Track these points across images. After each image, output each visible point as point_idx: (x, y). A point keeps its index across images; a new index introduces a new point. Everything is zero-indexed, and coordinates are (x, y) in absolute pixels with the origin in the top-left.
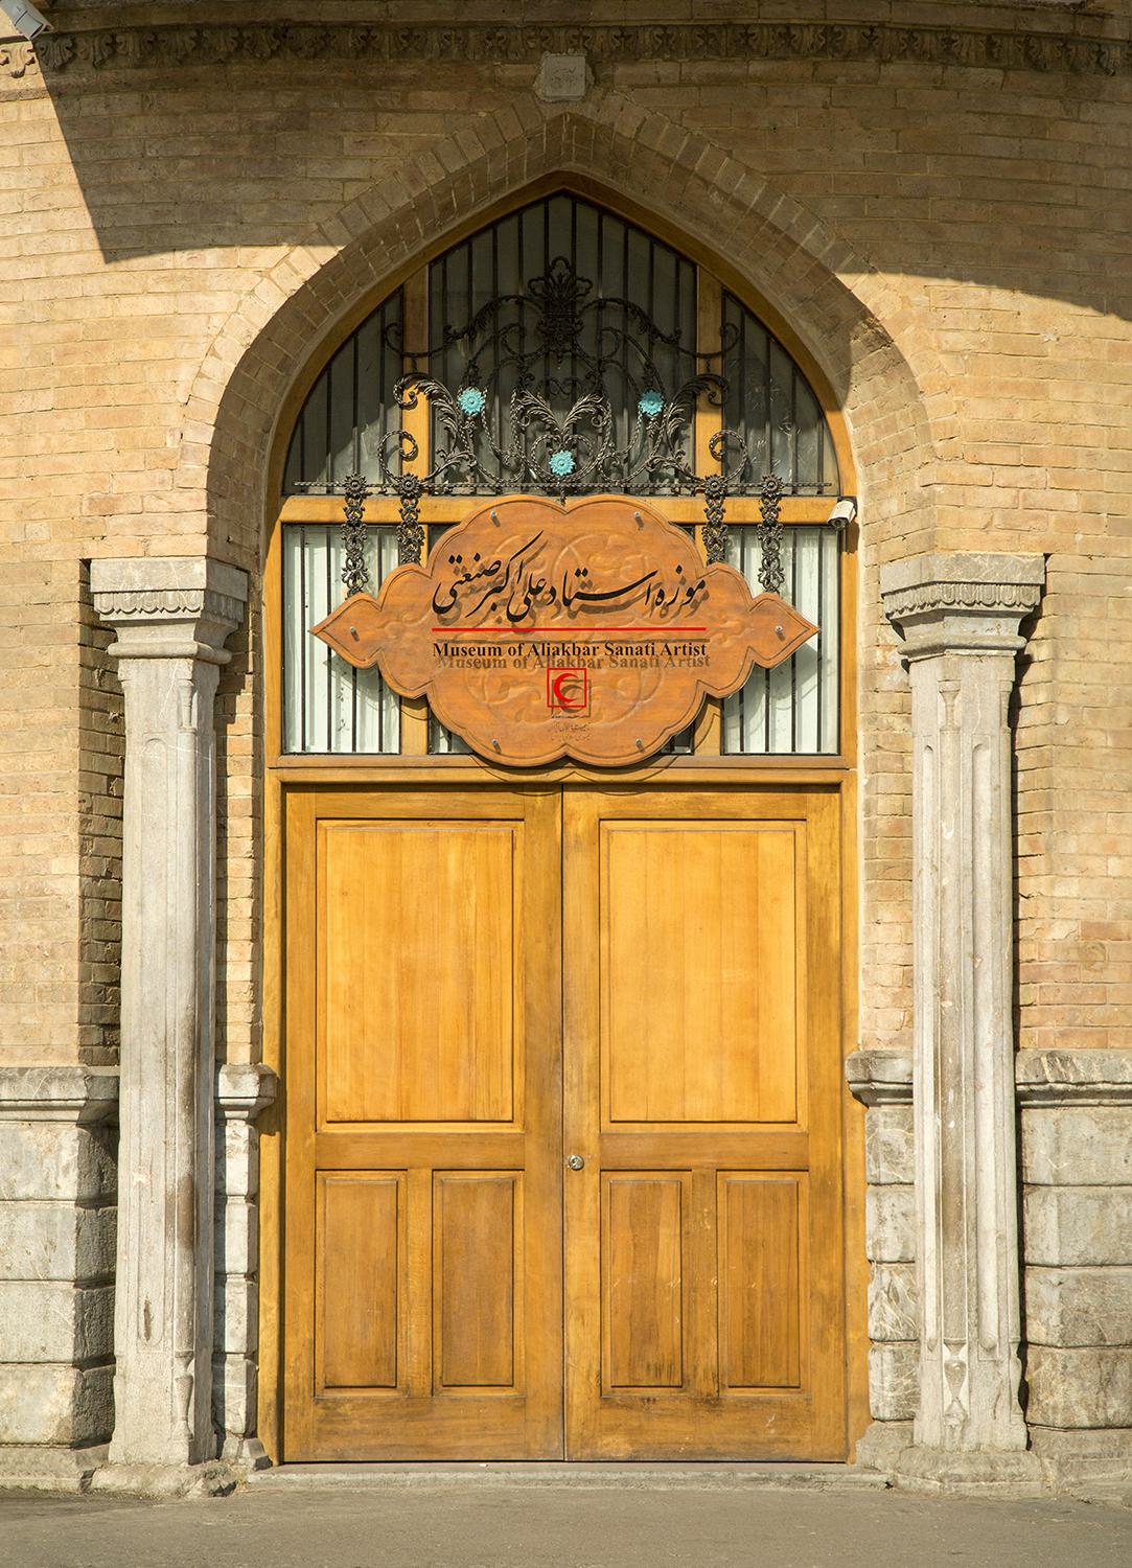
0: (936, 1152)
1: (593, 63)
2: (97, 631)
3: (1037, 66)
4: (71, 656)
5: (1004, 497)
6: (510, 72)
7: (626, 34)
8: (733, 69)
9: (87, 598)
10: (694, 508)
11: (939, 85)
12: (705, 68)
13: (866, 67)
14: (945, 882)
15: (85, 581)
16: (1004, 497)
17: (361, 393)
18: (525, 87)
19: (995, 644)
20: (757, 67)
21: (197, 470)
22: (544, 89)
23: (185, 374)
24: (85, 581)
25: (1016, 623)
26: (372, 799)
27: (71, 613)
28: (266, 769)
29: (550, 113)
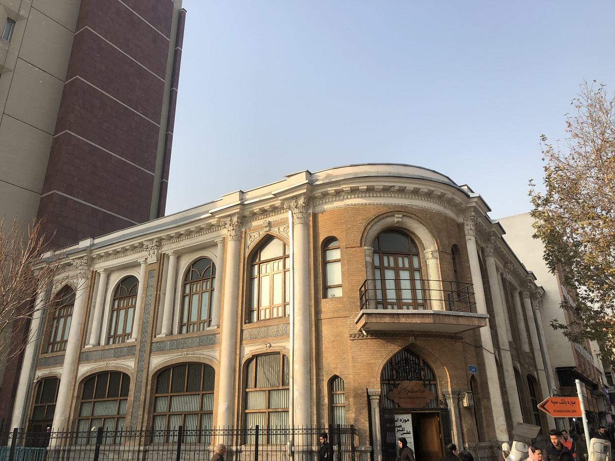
0: (223, 314)
2: (368, 396)
3: (453, 339)
4: (366, 399)
7: (418, 335)
8: (427, 339)
9: (367, 392)
10: (422, 382)
11: (445, 340)
12: (424, 339)
15: (367, 391)
17: (388, 166)
18: (408, 340)
19: (544, 342)
20: (430, 338)
21: (379, 379)
23: (377, 368)
24: (367, 391)
26: (292, 185)
27: (366, 394)
28: (412, 432)
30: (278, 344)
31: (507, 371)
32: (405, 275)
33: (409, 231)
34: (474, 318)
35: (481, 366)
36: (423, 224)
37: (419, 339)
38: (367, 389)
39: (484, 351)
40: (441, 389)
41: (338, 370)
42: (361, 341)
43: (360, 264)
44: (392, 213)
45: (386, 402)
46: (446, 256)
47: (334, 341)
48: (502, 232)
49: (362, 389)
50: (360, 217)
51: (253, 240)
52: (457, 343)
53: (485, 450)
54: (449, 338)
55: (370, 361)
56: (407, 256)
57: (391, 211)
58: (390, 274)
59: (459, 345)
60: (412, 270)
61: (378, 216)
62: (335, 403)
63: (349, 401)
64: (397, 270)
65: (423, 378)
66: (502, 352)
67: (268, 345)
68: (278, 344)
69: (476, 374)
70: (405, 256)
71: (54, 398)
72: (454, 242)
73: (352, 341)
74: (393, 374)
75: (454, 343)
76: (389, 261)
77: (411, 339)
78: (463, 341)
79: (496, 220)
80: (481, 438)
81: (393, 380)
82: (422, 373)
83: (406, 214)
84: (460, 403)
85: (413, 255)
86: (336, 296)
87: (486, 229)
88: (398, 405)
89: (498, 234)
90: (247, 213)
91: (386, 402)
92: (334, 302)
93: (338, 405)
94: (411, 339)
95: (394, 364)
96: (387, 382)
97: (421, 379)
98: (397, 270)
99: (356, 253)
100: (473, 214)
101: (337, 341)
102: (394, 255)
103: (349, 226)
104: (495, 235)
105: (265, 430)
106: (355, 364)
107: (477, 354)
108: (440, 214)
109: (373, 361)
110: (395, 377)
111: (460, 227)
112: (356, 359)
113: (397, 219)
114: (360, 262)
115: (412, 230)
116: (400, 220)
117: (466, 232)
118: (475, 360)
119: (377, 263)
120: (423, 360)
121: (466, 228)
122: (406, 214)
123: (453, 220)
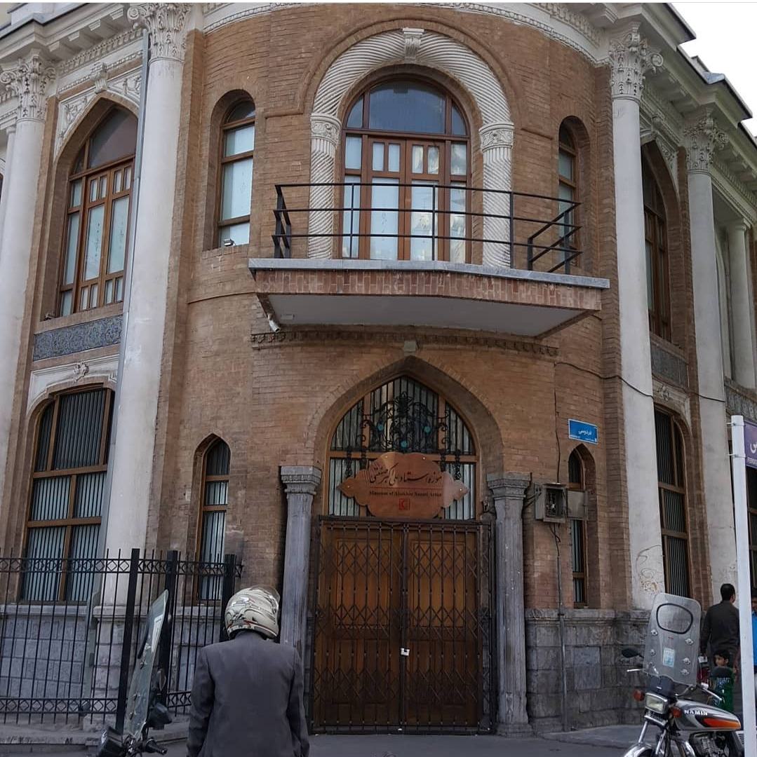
1: (418, 343)
5: (520, 457)
6: (397, 345)
9: (280, 476)
10: (438, 457)
11: (503, 353)
13: (486, 348)
14: (506, 560)
16: (520, 457)
18: (400, 349)
22: (405, 349)
25: (523, 491)
27: (275, 480)
29: (407, 355)
30: (103, 367)
31: (710, 450)
32: (422, 197)
33: (445, 76)
34: (562, 289)
35: (613, 426)
36: (480, 56)
37: (430, 346)
38: (280, 467)
39: (626, 390)
40: (485, 476)
41: (220, 423)
42: (277, 350)
43: (298, 157)
44: (396, 25)
45: (337, 502)
46: (536, 142)
47: (217, 354)
48: (741, 112)
49: (267, 469)
50: (308, 36)
51: (72, 117)
52: (538, 362)
53: (592, 629)
54: (515, 348)
55: (294, 401)
56: (438, 144)
57: (392, 16)
58: (385, 196)
59: (544, 369)
60: (444, 184)
61: (356, 31)
62: (212, 503)
63: (236, 498)
64: (405, 183)
65: (441, 446)
66: (704, 404)
67: (83, 368)
68: (103, 367)
69: (593, 445)
70: (432, 144)
71: (225, 548)
72: (571, 109)
73: (256, 352)
74: (362, 435)
75: (530, 361)
76: (386, 157)
77: (410, 347)
78: (558, 358)
79: (719, 75)
80: (584, 597)
81: (363, 450)
82: (442, 435)
83: (432, 26)
84: (530, 510)
85: (453, 142)
86: (237, 243)
87: (689, 97)
88: (368, 511)
89: (730, 118)
90: (54, 46)
91: (337, 502)
92: (227, 258)
93: (213, 508)
94: (410, 347)
95: (367, 411)
96: (344, 454)
97: (436, 450)
98: (405, 183)
99: (290, 128)
100: (636, 37)
101: (225, 352)
102: (403, 143)
103: (279, 59)
104: (717, 116)
105: (63, 560)
106: (257, 407)
107: (606, 396)
108: (538, 32)
109: (302, 400)
110: (366, 444)
111: (600, 77)
112: (261, 396)
113: (413, 36)
114: (298, 153)
115: (452, 74)
116: (417, 42)
117: (615, 91)
118: (596, 409)
119: (353, 160)
120: (447, 403)
121: (617, 79)
122: (432, 26)
123: (578, 55)
